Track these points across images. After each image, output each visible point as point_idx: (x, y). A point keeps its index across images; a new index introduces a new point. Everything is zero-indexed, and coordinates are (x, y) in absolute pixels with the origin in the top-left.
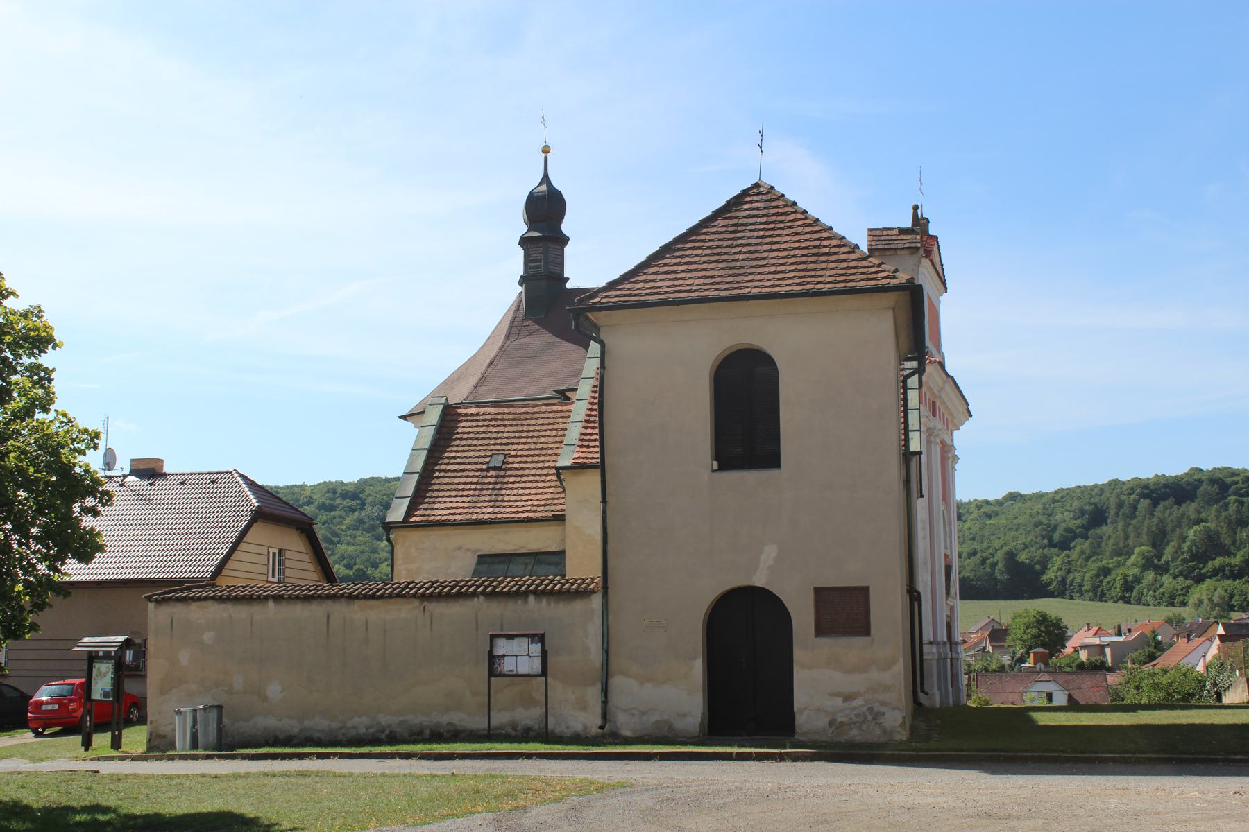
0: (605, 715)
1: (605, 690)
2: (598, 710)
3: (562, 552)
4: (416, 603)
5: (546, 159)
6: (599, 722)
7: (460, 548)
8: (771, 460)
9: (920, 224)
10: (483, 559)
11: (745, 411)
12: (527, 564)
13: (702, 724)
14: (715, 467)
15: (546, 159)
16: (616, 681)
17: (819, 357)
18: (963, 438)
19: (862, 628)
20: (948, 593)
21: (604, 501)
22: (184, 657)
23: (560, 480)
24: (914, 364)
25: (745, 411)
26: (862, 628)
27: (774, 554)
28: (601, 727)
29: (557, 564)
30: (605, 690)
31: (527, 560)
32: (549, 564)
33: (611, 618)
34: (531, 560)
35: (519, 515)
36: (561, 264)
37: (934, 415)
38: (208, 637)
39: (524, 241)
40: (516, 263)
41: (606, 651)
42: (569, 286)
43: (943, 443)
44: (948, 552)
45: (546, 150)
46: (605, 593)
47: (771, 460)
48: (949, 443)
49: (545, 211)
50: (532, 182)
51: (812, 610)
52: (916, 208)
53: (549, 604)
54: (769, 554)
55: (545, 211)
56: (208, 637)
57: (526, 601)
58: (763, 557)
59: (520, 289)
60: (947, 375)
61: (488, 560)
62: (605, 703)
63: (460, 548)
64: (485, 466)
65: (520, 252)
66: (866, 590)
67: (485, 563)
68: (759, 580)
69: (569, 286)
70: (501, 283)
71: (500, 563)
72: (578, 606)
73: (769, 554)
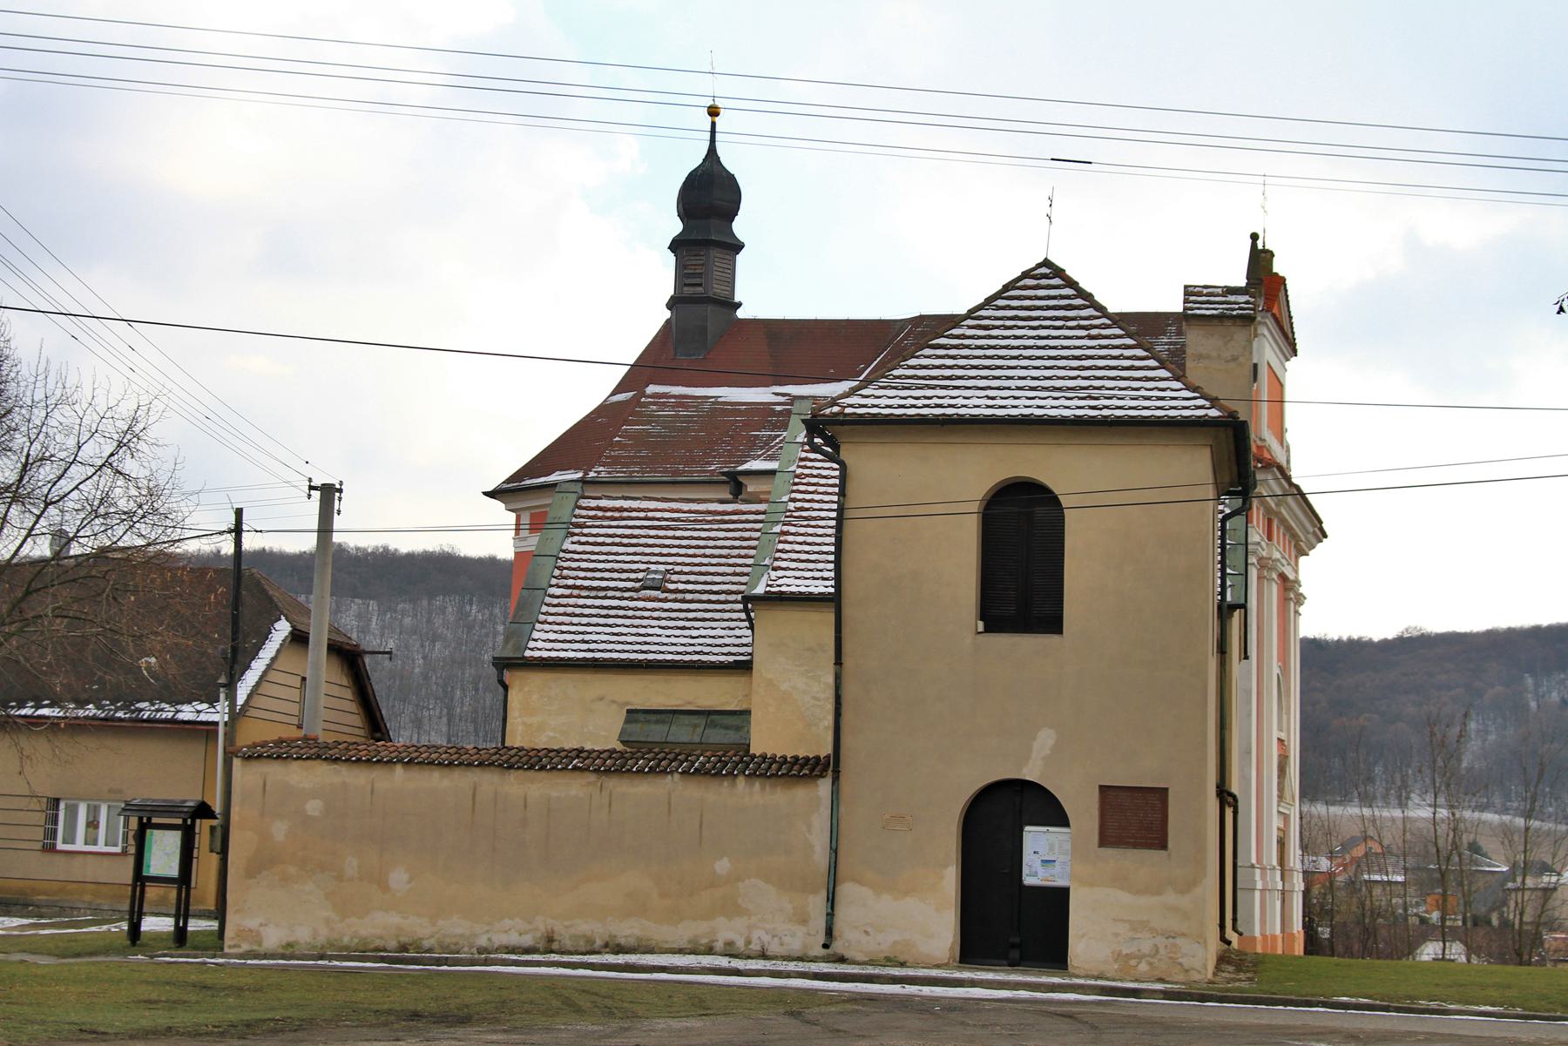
0: (829, 932)
1: (832, 900)
2: (821, 924)
3: (748, 712)
4: (592, 777)
5: (713, 124)
6: (822, 939)
7: (601, 699)
8: (1052, 623)
9: (1260, 259)
10: (633, 715)
11: (1021, 565)
12: (696, 726)
13: (951, 948)
14: (981, 629)
15: (713, 124)
16: (846, 890)
17: (1120, 524)
18: (1312, 570)
19: (1156, 838)
20: (1281, 797)
21: (838, 662)
22: (279, 830)
23: (749, 619)
24: (1238, 502)
25: (1021, 565)
26: (1156, 838)
27: (1051, 742)
28: (825, 946)
29: (738, 729)
30: (832, 900)
31: (695, 720)
32: (727, 728)
33: (842, 809)
34: (701, 721)
35: (687, 658)
36: (731, 283)
37: (1270, 538)
38: (314, 807)
39: (675, 246)
40: (661, 277)
41: (835, 851)
42: (741, 314)
43: (1283, 577)
44: (1283, 736)
45: (713, 112)
46: (836, 779)
47: (1052, 623)
48: (1291, 577)
49: (709, 201)
50: (695, 158)
51: (1096, 813)
52: (1254, 237)
53: (763, 788)
54: (1045, 740)
55: (709, 201)
56: (314, 807)
57: (734, 785)
58: (1036, 745)
59: (668, 314)
60: (1291, 484)
61: (641, 717)
62: (831, 915)
63: (601, 699)
64: (638, 585)
65: (671, 258)
66: (1164, 792)
67: (636, 721)
68: (1030, 774)
69: (741, 314)
70: (641, 301)
71: (657, 722)
72: (800, 793)
73: (1045, 740)
